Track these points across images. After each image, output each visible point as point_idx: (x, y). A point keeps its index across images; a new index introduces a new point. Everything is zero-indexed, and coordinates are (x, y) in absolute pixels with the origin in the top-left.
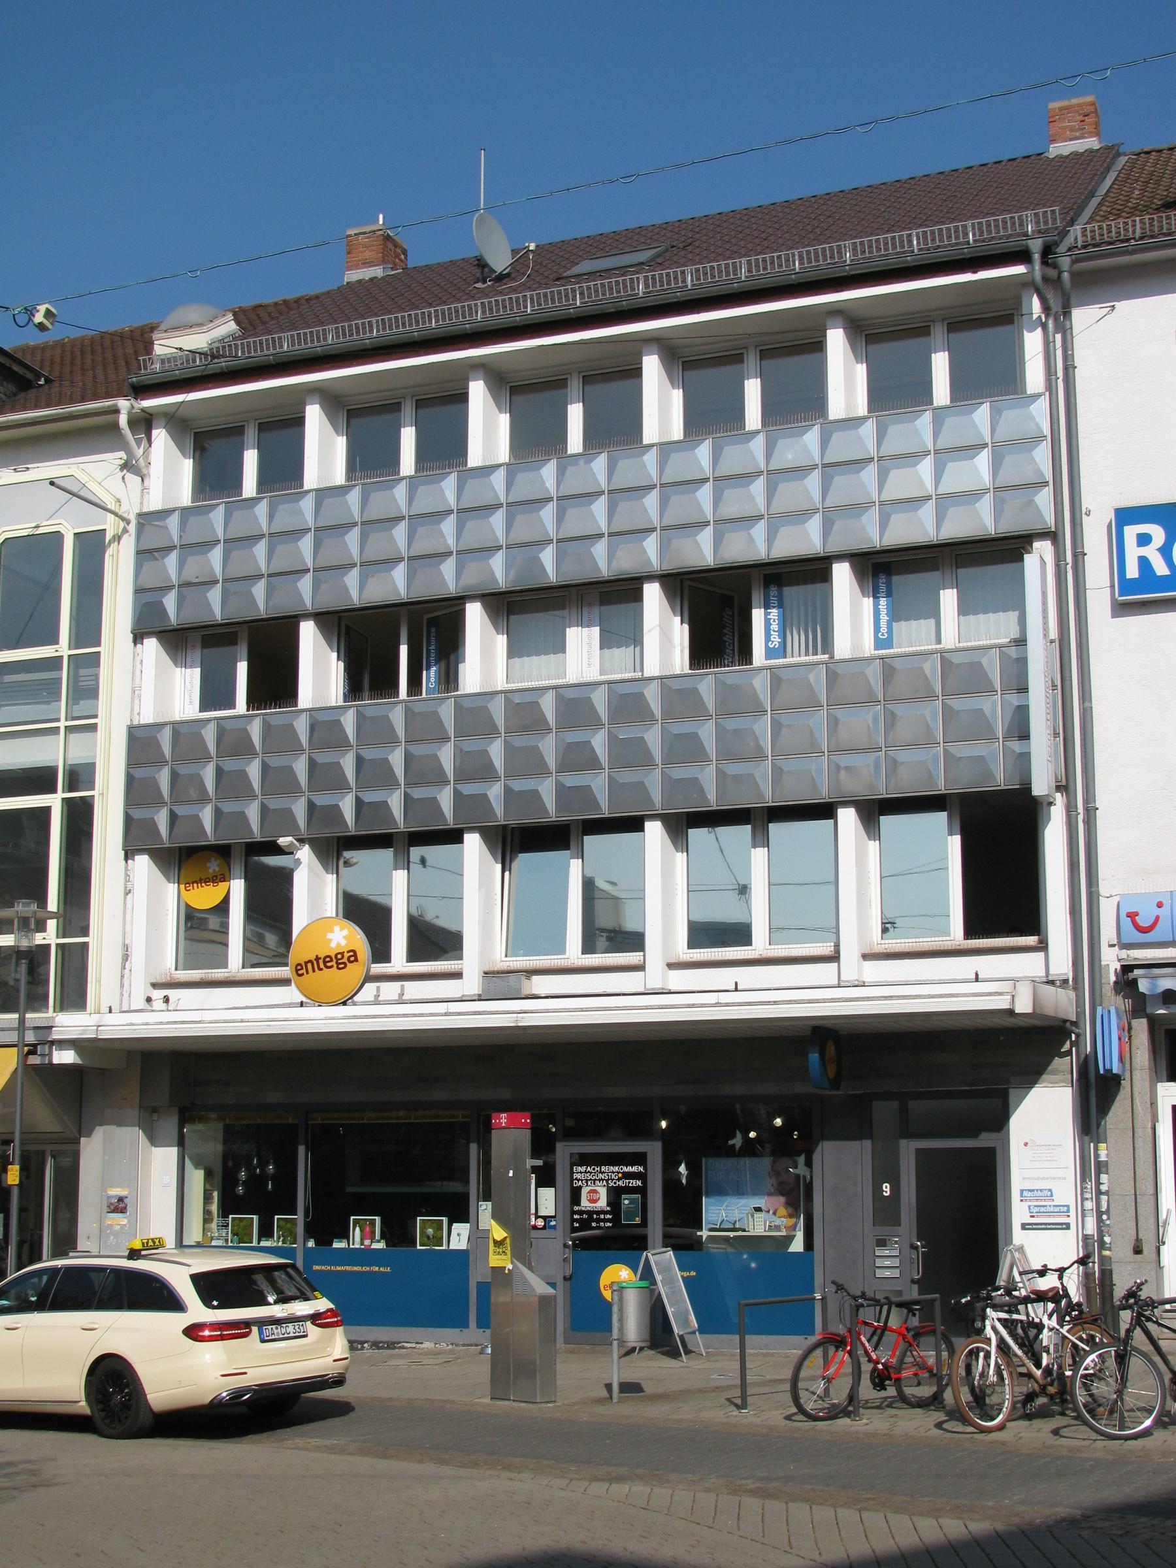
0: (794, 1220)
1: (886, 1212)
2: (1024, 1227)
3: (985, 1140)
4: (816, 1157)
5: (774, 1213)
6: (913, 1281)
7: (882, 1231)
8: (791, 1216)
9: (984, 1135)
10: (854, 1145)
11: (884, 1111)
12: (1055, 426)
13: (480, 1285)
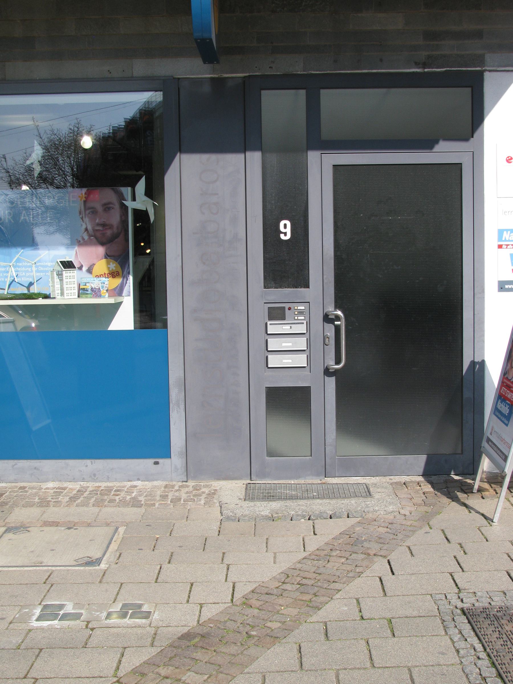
0: (117, 281)
1: (285, 266)
2: (502, 286)
3: (444, 153)
4: (170, 179)
5: (90, 271)
6: (327, 372)
7: (280, 295)
8: (113, 275)
9: (442, 146)
10: (233, 161)
11: (281, 108)
12: (495, 449)
13: (129, 295)
